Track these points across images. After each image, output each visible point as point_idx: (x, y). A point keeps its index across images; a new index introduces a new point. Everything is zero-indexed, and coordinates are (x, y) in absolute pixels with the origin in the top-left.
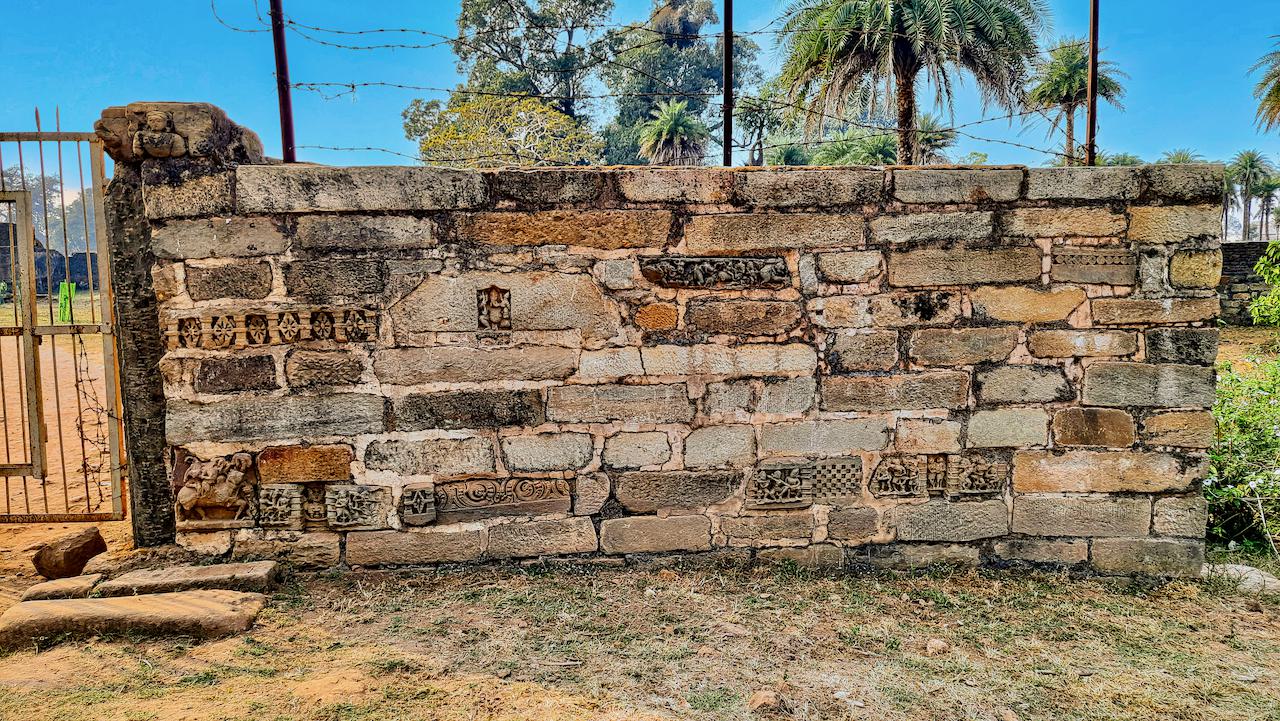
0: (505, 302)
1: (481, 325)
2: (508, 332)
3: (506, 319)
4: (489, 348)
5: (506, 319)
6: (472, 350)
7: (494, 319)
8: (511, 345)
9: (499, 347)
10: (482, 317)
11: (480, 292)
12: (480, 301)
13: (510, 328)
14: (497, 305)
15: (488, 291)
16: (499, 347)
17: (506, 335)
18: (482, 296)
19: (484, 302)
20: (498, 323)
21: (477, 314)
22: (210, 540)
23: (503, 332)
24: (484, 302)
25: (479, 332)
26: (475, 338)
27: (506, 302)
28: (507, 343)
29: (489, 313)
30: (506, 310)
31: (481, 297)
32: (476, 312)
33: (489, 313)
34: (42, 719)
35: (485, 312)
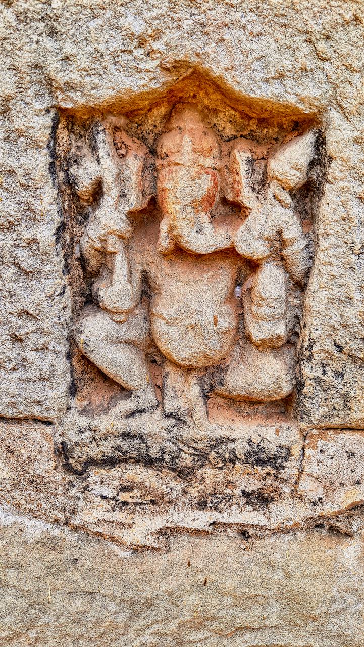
0: (268, 217)
1: (88, 373)
2: (273, 434)
3: (270, 346)
4: (143, 528)
5: (270, 346)
6: (36, 529)
7: (177, 343)
8: (284, 511)
9: (202, 519)
10: (95, 328)
11: (75, 122)
12: (80, 204)
13: (287, 406)
14: (205, 238)
15: (140, 122)
16: (202, 519)
17: (258, 458)
18: (98, 166)
19: (110, 218)
20: (210, 374)
21: (56, 312)
22: (112, 362)
23: (245, 431)
24: (110, 218)
25: (74, 426)
26: (46, 466)
27: (286, 219)
28: (260, 499)
29: (147, 290)
30: (270, 282)
31: (85, 174)
32: (49, 291)
33: (147, 290)
34: (100, 645)
35: (117, 289)
